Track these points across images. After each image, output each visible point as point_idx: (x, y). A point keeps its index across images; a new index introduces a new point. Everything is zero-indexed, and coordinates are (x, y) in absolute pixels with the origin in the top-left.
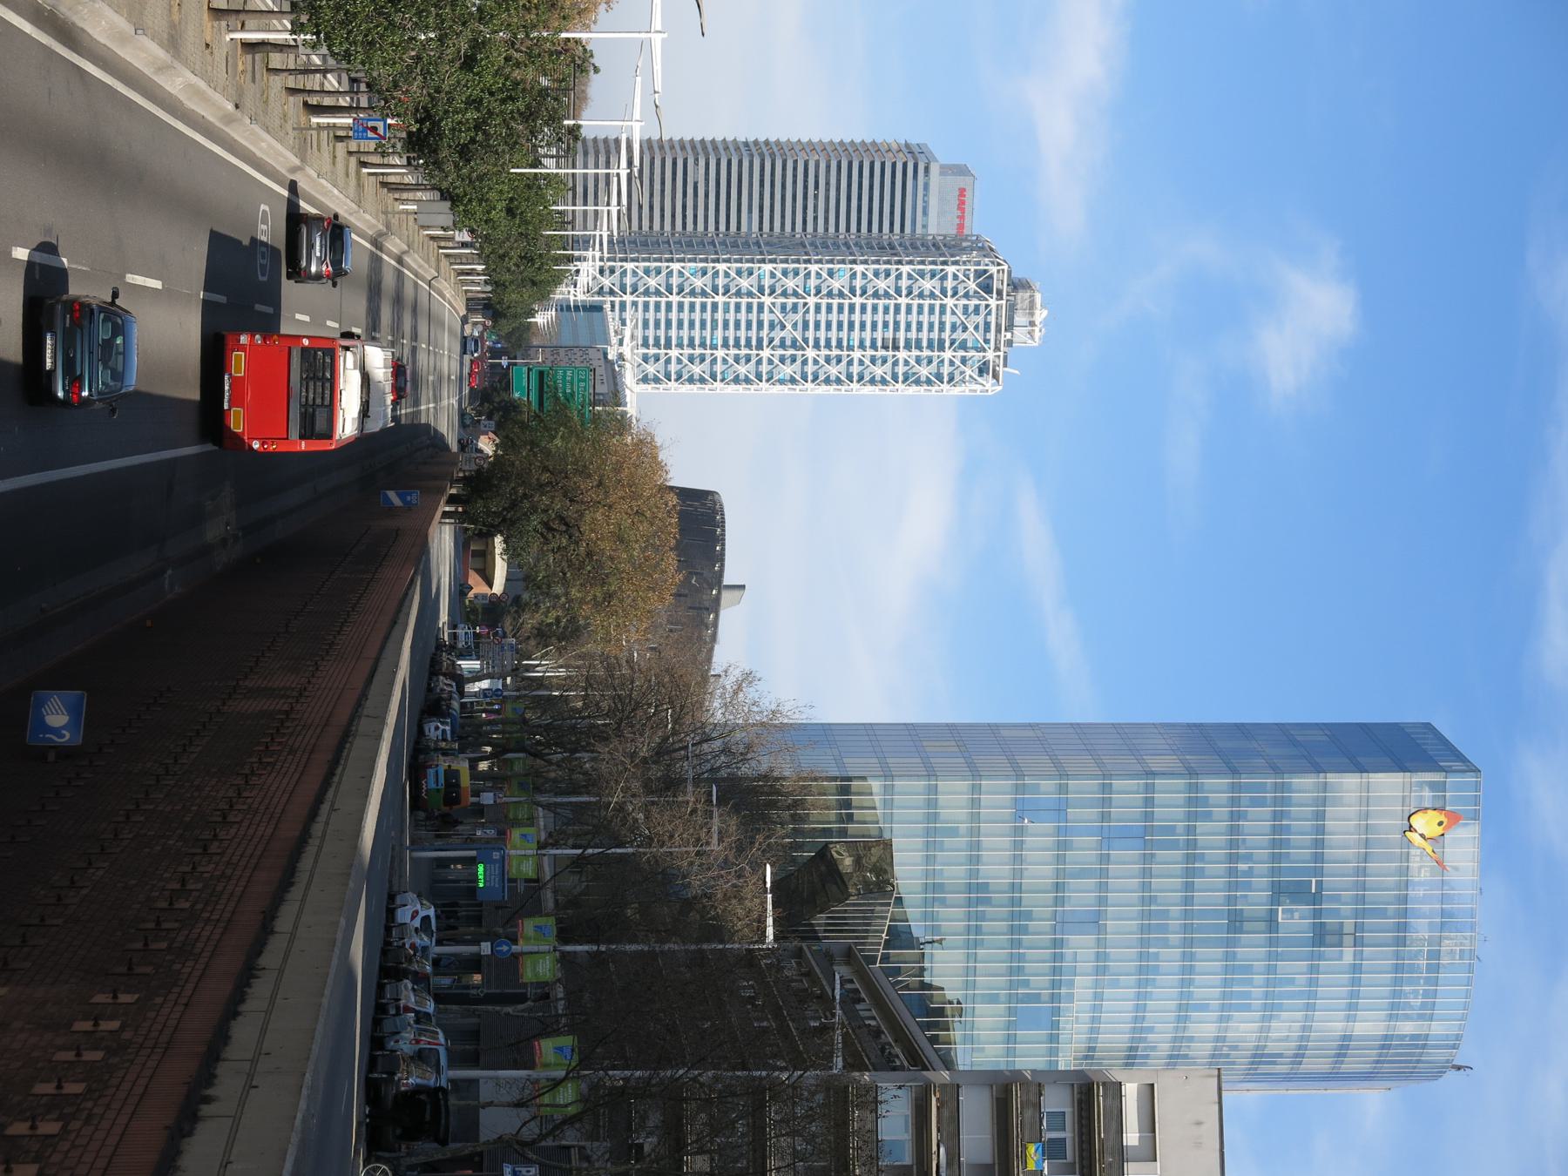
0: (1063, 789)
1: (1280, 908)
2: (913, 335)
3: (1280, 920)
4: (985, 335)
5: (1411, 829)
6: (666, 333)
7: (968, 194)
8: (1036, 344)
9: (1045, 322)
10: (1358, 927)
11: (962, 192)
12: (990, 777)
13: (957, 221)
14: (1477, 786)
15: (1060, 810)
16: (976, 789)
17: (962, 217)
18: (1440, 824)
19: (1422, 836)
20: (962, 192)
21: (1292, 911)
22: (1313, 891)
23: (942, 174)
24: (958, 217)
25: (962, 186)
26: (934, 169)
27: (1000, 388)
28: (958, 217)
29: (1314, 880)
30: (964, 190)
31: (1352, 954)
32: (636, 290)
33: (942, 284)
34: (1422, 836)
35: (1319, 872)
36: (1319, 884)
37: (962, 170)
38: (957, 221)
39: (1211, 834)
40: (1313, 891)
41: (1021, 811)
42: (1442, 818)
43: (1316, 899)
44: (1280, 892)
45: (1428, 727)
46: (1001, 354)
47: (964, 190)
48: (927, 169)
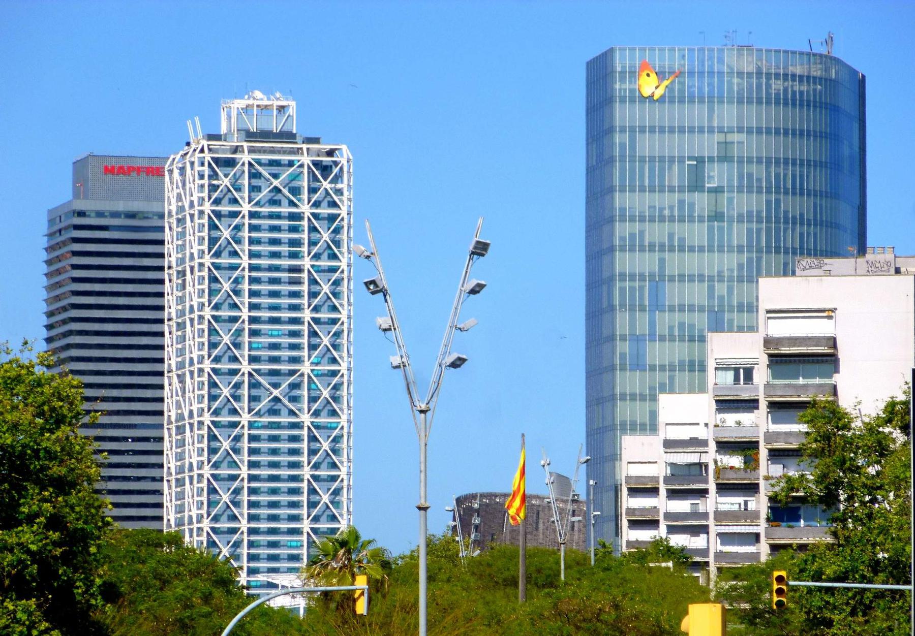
0: (623, 338)
1: (707, 185)
2: (284, 249)
3: (716, 185)
4: (284, 165)
5: (652, 95)
6: (284, 480)
7: (110, 163)
8: (293, 104)
9: (268, 93)
10: (721, 130)
11: (108, 170)
12: (613, 388)
13: (143, 175)
14: (623, 50)
15: (638, 340)
16: (623, 397)
17: (139, 170)
18: (648, 75)
19: (657, 88)
20: (108, 170)
21: (709, 177)
22: (695, 163)
23: (86, 197)
24: (138, 175)
25: (103, 169)
26: (80, 205)
27: (344, 148)
28: (138, 175)
29: (688, 163)
30: (106, 168)
31: (739, 134)
32: (215, 427)
33: (225, 216)
34: (657, 88)
35: (682, 160)
36: (690, 158)
37: (80, 166)
38: (143, 175)
39: (656, 232)
40: (695, 163)
41: (638, 365)
42: (644, 74)
43: (700, 160)
44: (696, 185)
45: (588, 63)
46: (305, 147)
47: (106, 168)
48: (81, 214)
